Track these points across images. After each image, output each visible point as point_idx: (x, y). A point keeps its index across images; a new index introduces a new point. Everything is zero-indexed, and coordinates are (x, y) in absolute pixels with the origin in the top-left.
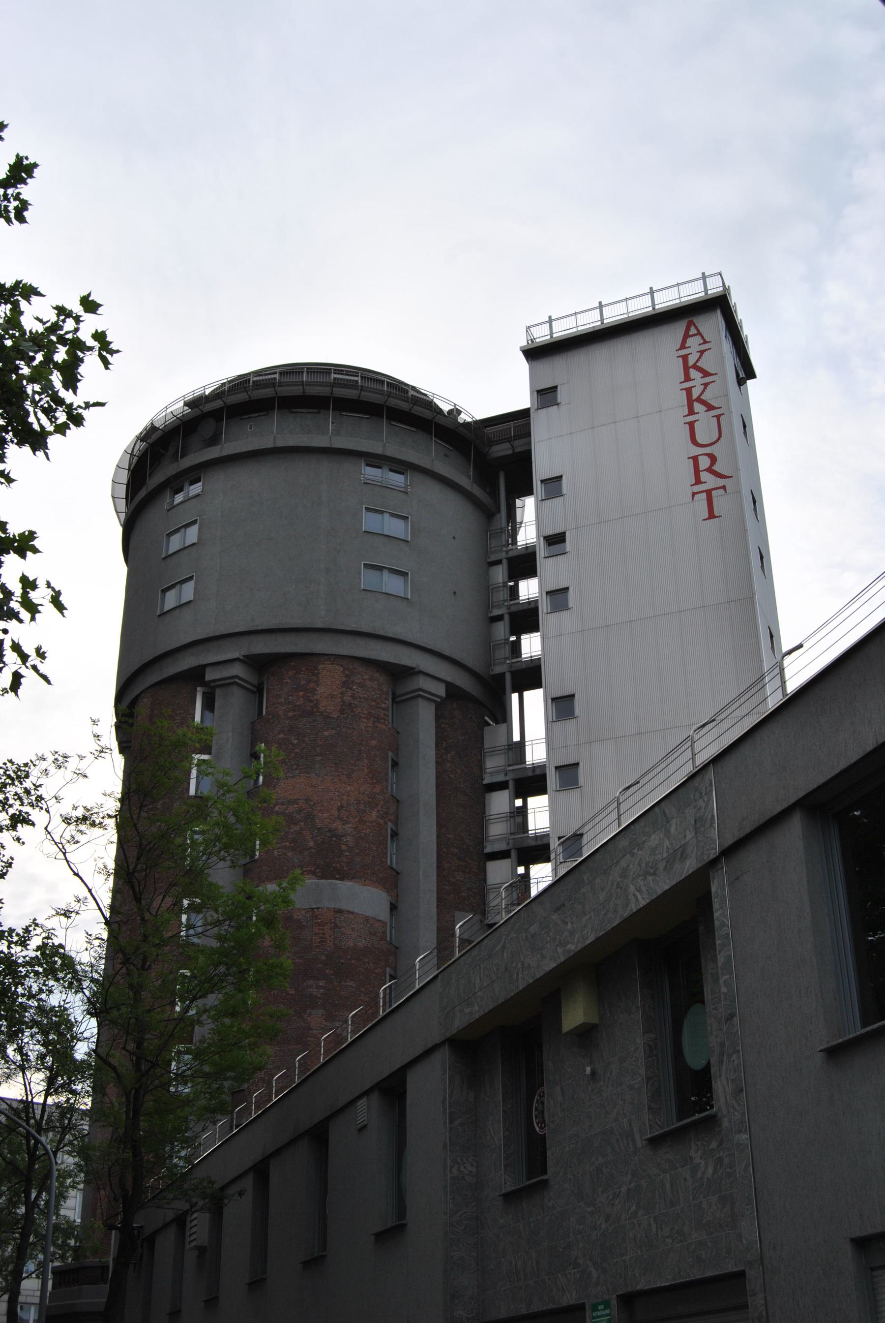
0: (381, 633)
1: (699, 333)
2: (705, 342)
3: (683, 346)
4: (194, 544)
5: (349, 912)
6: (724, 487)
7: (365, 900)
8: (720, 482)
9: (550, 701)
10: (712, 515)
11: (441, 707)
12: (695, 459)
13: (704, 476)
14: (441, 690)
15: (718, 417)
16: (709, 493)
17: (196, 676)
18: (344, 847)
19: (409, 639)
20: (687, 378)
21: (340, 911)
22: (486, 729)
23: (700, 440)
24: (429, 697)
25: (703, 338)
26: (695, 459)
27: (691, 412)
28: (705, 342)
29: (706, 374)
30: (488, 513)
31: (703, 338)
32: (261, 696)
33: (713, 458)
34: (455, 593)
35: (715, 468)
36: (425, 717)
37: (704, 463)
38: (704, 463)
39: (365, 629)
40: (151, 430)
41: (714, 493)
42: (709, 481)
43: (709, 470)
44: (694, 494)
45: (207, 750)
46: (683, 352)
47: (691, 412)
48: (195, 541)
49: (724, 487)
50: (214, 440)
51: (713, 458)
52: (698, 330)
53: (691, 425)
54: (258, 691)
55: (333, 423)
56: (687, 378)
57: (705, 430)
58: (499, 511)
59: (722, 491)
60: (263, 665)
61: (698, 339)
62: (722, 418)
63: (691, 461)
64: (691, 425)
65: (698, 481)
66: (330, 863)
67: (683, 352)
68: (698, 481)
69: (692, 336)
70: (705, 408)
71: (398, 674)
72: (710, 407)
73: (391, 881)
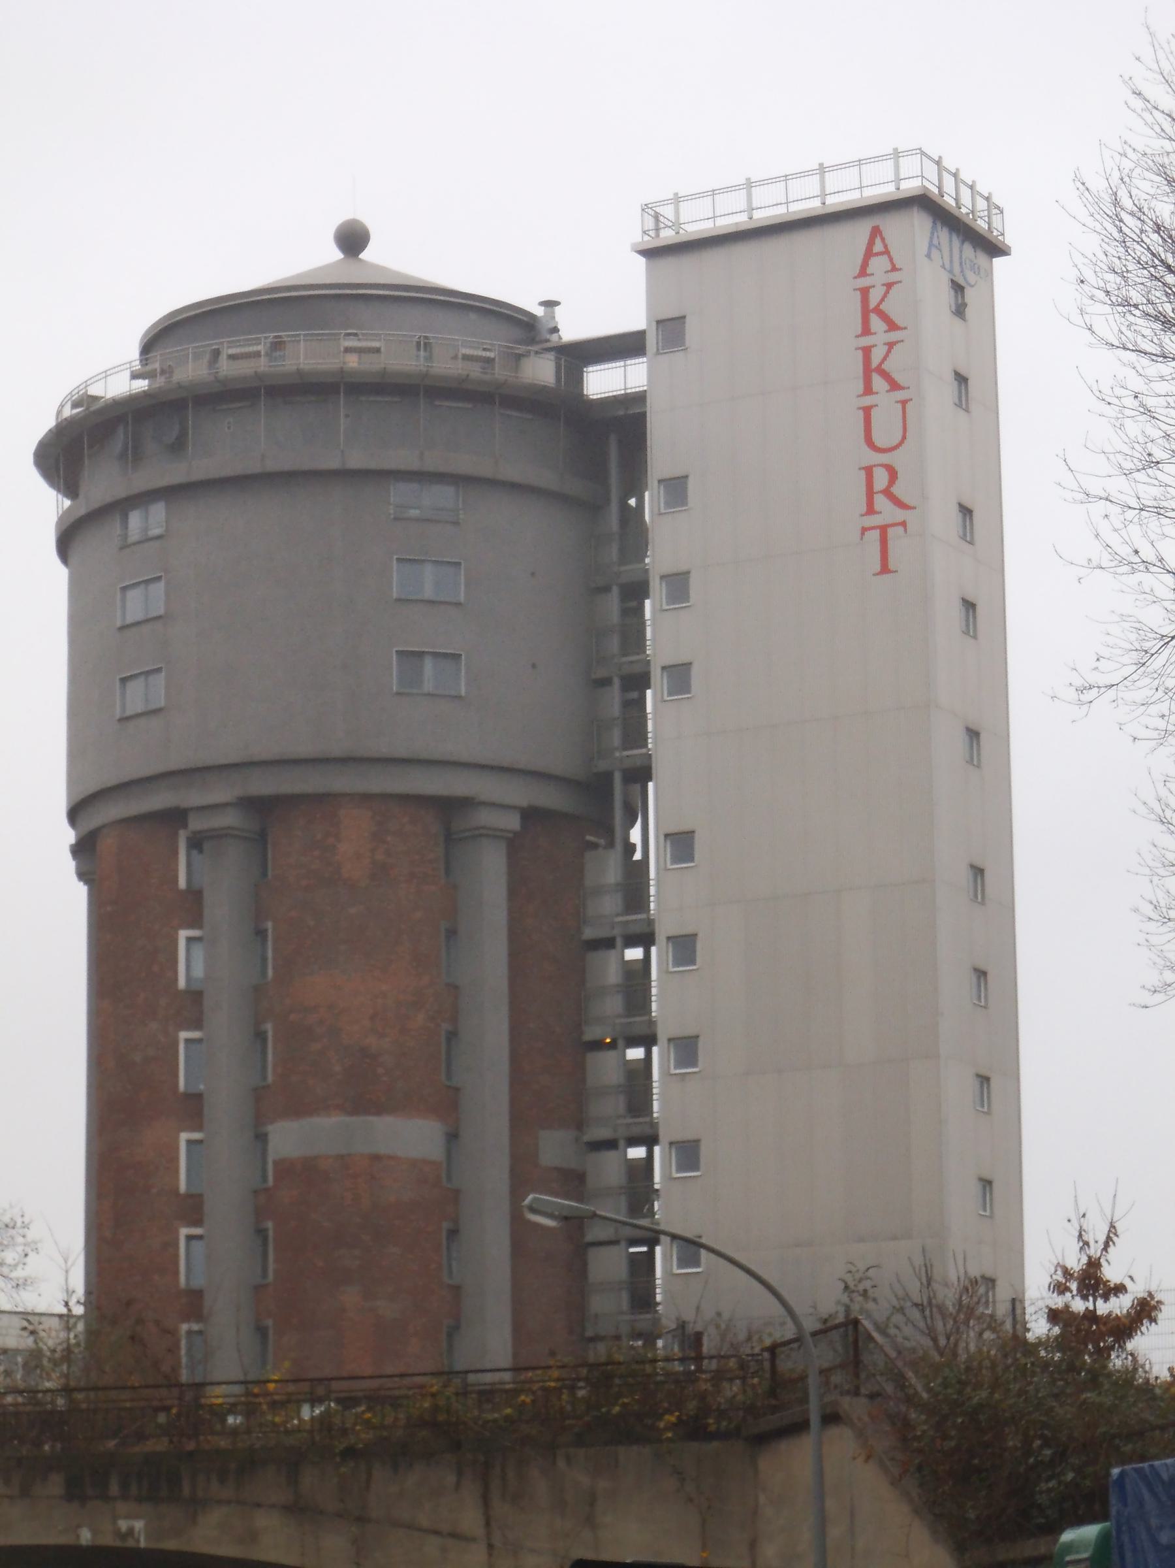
0: (424, 755)
1: (886, 252)
2: (894, 269)
3: (863, 272)
4: (159, 618)
5: (390, 1157)
6: (903, 524)
7: (411, 1137)
8: (900, 515)
9: (662, 838)
10: (885, 569)
11: (514, 844)
12: (869, 471)
13: (881, 502)
14: (513, 822)
15: (904, 403)
16: (884, 530)
17: (176, 817)
18: (380, 1070)
19: (465, 757)
20: (866, 331)
21: (376, 1158)
22: (589, 855)
23: (879, 441)
24: (494, 834)
25: (891, 260)
26: (869, 471)
27: (868, 390)
28: (894, 269)
29: (892, 326)
30: (590, 508)
31: (891, 260)
32: (265, 849)
33: (893, 474)
34: (534, 666)
35: (895, 490)
36: (490, 872)
37: (881, 479)
38: (881, 479)
39: (402, 752)
40: (84, 400)
41: (890, 531)
42: (887, 511)
43: (887, 493)
44: (864, 530)
45: (197, 1024)
46: (864, 282)
47: (868, 390)
48: (161, 612)
49: (903, 524)
50: (178, 447)
51: (893, 474)
52: (886, 246)
53: (867, 411)
54: (261, 839)
55: (347, 416)
56: (866, 331)
57: (885, 431)
58: (608, 501)
59: (900, 529)
60: (265, 810)
61: (884, 259)
62: (909, 406)
63: (863, 472)
64: (867, 411)
65: (871, 510)
66: (365, 1095)
67: (864, 282)
68: (871, 510)
69: (877, 254)
70: (886, 386)
71: (449, 807)
72: (894, 386)
73: (447, 1105)
